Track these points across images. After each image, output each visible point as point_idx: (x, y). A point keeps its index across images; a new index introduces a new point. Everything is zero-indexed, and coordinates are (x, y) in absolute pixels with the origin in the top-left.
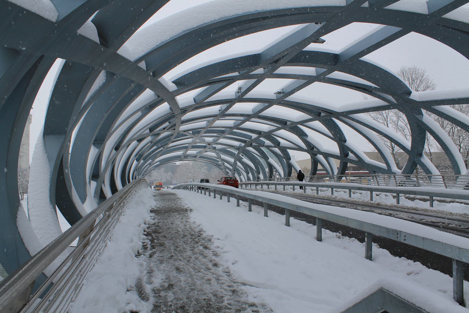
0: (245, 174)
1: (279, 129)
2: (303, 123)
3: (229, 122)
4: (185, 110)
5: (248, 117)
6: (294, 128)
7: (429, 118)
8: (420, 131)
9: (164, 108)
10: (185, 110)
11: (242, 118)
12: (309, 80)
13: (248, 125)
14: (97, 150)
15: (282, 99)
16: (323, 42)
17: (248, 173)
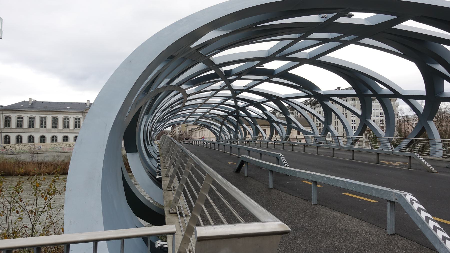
0: (229, 134)
1: (249, 105)
2: (263, 102)
3: (218, 100)
4: (189, 95)
5: (209, 98)
6: (258, 105)
7: (329, 104)
8: (328, 112)
9: (180, 96)
10: (189, 95)
11: (206, 98)
12: (262, 81)
13: (210, 101)
14: (137, 155)
15: (248, 89)
16: (263, 66)
17: (230, 133)
